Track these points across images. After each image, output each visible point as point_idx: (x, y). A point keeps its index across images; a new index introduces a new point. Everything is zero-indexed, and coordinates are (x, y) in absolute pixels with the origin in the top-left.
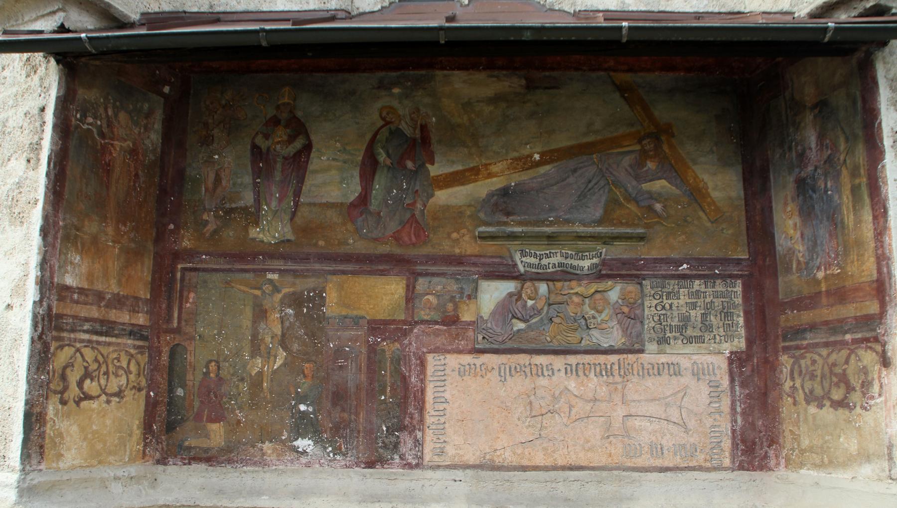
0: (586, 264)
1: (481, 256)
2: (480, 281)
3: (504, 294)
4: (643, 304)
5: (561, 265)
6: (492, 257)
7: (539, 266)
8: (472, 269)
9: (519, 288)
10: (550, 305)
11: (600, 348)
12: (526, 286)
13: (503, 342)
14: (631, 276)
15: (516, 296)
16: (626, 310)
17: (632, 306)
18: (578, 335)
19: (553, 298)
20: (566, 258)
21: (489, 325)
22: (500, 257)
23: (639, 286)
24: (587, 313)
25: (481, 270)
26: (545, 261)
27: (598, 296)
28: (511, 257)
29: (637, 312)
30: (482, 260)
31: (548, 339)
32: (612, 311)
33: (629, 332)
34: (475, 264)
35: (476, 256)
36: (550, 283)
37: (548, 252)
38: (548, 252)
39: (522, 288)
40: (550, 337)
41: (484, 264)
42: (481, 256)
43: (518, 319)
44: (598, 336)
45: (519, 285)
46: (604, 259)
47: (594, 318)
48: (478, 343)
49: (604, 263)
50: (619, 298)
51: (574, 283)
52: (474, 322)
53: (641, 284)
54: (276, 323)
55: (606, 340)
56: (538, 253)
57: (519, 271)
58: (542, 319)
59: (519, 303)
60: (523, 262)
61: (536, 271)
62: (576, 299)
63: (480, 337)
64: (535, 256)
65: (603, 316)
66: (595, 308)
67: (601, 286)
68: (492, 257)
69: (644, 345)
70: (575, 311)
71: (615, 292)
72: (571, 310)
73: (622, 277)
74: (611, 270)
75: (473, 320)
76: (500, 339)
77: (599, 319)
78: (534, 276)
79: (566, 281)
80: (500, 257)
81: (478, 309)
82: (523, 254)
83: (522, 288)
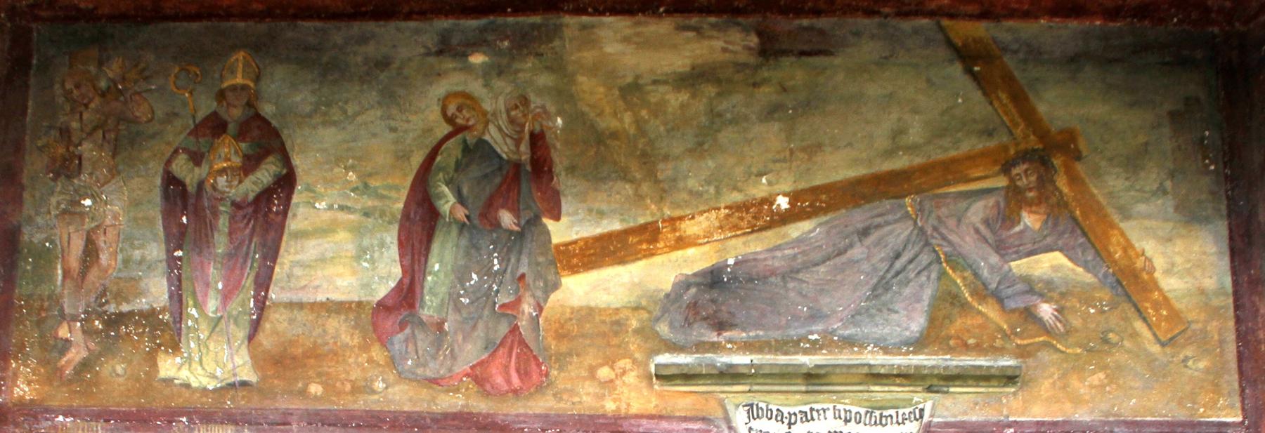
1: (661, 417)
6: (685, 419)
20: (847, 421)
22: (703, 419)
35: (651, 417)
37: (806, 408)
42: (661, 417)
46: (929, 424)
56: (785, 410)
64: (779, 328)
68: (685, 419)
80: (703, 419)
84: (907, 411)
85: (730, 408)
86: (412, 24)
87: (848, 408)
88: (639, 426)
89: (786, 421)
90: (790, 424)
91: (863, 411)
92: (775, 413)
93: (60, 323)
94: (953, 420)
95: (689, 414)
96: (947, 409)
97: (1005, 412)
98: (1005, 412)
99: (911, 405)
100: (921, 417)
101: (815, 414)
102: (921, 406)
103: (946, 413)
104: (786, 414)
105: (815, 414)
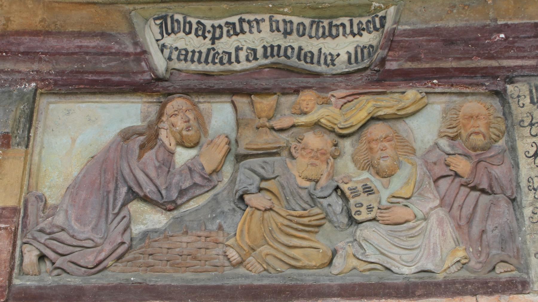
0: (342, 47)
1: (48, 33)
2: (43, 102)
3: (112, 132)
4: (513, 149)
5: (270, 50)
6: (80, 35)
7: (211, 56)
8: (23, 67)
9: (153, 116)
10: (240, 158)
11: (390, 279)
12: (170, 108)
13: (98, 267)
14: (472, 72)
15: (148, 137)
16: (463, 166)
17: (479, 154)
18: (322, 241)
19: (250, 140)
20: (286, 33)
21: (60, 219)
22: (102, 35)
23: (496, 102)
24: (348, 179)
25: (45, 68)
26: (226, 44)
27: (378, 130)
28: (133, 34)
29: (497, 171)
30: (52, 43)
31: (233, 255)
32: (420, 170)
33: (475, 230)
34: (30, 55)
35: (36, 33)
36: (242, 101)
37: (235, 19)
38: (235, 19)
39: (161, 114)
40: (238, 248)
41: (54, 54)
42: (48, 33)
43: (146, 199)
44: (385, 246)
45: (154, 109)
46: (393, 32)
47: (368, 190)
48: (22, 273)
49: (392, 42)
50: (441, 135)
51: (307, 98)
52: (15, 210)
53: (500, 94)
54: (41, 14)
55: (407, 255)
56: (208, 23)
57: (152, 69)
58: (215, 198)
59: (150, 155)
60: (162, 49)
61: (201, 67)
62: (314, 141)
63: (31, 256)
64: (201, 31)
65: (397, 185)
66: (370, 166)
67: (387, 104)
68: (80, 35)
69: (526, 268)
70: (311, 172)
71: (429, 119)
72: (299, 171)
73: (443, 74)
74: (414, 58)
75: (11, 203)
76: (90, 258)
77: (385, 195)
78: (194, 82)
79: (285, 92)
80: (102, 35)
81: (30, 172)
82: (167, 26)
83: (161, 114)
84: (364, 20)
85: (137, 21)
86: (136, 26)
87: (288, 18)
88: (19, 44)
89: (209, 36)
90: (213, 40)
91: (307, 22)
92: (194, 26)
93: (197, 107)
94: (424, 26)
95: (84, 29)
96: (416, 15)
97: (491, 15)
98: (491, 15)
99: (369, 13)
100: (383, 26)
101: (246, 27)
102: (380, 14)
103: (414, 19)
104: (208, 28)
105: (246, 27)
